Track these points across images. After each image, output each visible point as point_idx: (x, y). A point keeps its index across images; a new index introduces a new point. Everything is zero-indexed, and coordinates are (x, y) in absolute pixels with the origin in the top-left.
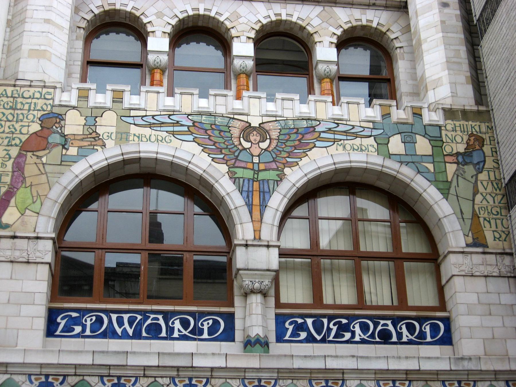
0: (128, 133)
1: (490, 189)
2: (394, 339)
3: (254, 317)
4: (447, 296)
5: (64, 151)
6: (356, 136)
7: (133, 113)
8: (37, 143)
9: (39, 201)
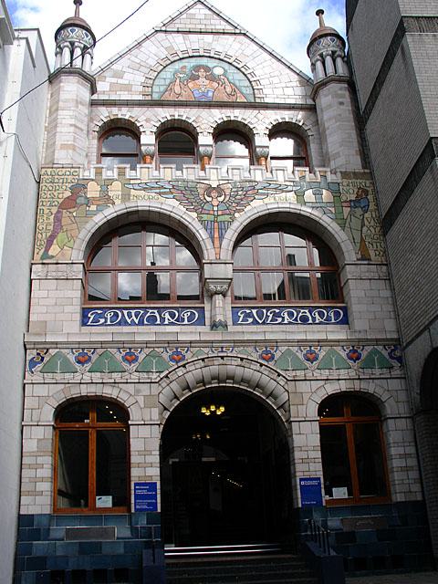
0: (129, 195)
1: (372, 223)
2: (310, 321)
7: (132, 182)
8: (69, 203)
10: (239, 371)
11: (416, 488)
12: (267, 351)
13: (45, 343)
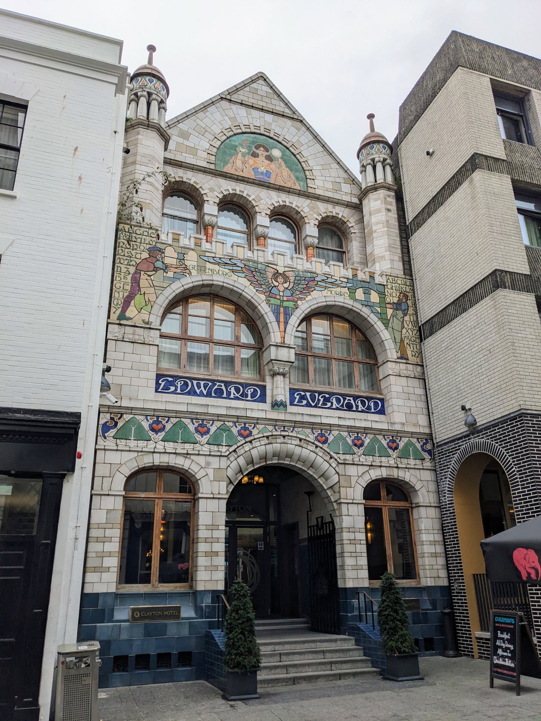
1: (410, 326)
2: (354, 409)
5: (165, 274)
6: (338, 286)
7: (207, 254)
10: (298, 450)
11: (443, 573)
12: (322, 433)
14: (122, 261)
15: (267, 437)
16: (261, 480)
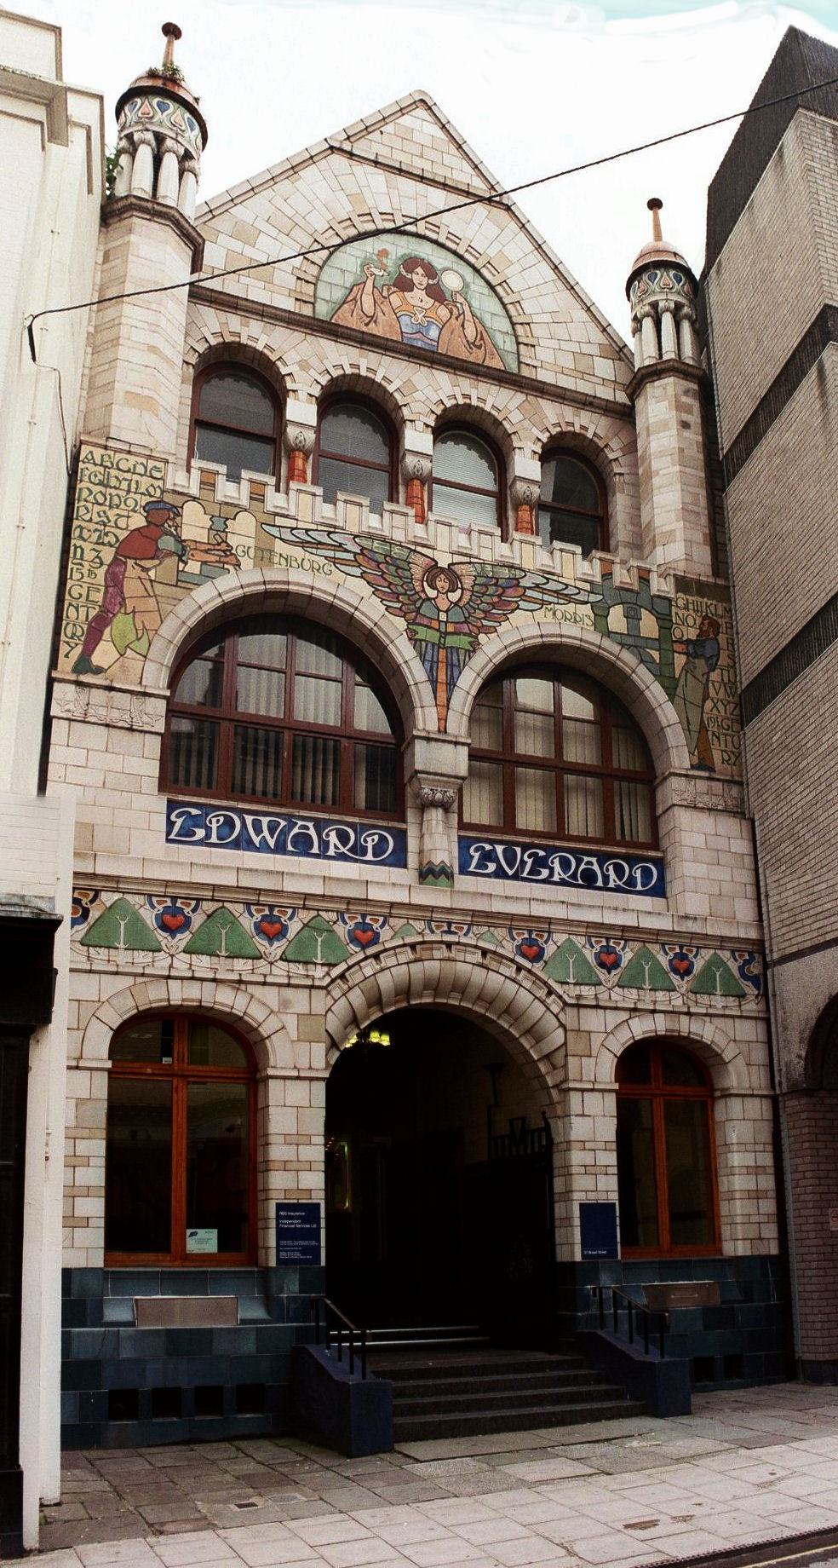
0: (271, 551)
2: (600, 883)
3: (437, 839)
4: (662, 832)
5: (181, 566)
6: (569, 599)
7: (279, 521)
9: (145, 640)
10: (479, 975)
11: (771, 1231)
12: (532, 936)
13: (94, 876)
14: (86, 534)
15: (413, 946)
16: (385, 1041)
